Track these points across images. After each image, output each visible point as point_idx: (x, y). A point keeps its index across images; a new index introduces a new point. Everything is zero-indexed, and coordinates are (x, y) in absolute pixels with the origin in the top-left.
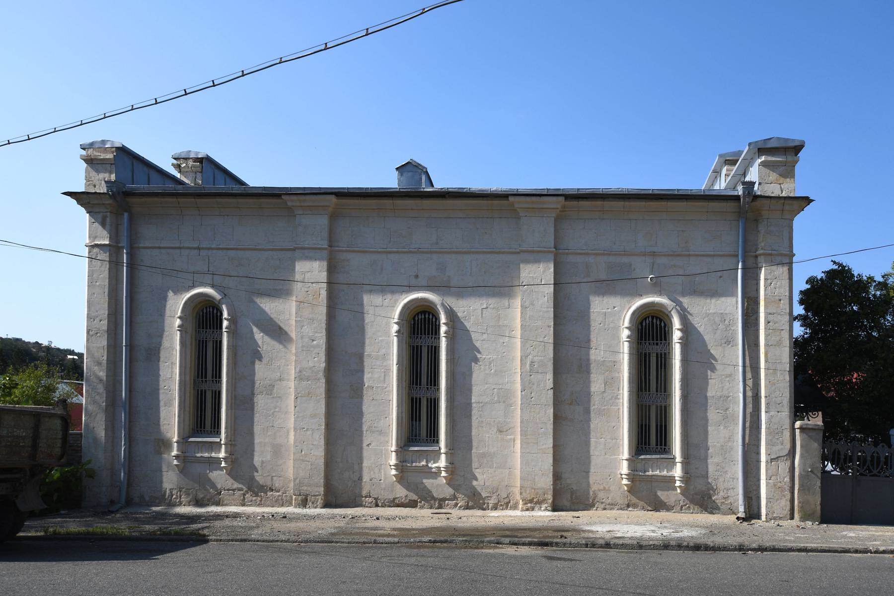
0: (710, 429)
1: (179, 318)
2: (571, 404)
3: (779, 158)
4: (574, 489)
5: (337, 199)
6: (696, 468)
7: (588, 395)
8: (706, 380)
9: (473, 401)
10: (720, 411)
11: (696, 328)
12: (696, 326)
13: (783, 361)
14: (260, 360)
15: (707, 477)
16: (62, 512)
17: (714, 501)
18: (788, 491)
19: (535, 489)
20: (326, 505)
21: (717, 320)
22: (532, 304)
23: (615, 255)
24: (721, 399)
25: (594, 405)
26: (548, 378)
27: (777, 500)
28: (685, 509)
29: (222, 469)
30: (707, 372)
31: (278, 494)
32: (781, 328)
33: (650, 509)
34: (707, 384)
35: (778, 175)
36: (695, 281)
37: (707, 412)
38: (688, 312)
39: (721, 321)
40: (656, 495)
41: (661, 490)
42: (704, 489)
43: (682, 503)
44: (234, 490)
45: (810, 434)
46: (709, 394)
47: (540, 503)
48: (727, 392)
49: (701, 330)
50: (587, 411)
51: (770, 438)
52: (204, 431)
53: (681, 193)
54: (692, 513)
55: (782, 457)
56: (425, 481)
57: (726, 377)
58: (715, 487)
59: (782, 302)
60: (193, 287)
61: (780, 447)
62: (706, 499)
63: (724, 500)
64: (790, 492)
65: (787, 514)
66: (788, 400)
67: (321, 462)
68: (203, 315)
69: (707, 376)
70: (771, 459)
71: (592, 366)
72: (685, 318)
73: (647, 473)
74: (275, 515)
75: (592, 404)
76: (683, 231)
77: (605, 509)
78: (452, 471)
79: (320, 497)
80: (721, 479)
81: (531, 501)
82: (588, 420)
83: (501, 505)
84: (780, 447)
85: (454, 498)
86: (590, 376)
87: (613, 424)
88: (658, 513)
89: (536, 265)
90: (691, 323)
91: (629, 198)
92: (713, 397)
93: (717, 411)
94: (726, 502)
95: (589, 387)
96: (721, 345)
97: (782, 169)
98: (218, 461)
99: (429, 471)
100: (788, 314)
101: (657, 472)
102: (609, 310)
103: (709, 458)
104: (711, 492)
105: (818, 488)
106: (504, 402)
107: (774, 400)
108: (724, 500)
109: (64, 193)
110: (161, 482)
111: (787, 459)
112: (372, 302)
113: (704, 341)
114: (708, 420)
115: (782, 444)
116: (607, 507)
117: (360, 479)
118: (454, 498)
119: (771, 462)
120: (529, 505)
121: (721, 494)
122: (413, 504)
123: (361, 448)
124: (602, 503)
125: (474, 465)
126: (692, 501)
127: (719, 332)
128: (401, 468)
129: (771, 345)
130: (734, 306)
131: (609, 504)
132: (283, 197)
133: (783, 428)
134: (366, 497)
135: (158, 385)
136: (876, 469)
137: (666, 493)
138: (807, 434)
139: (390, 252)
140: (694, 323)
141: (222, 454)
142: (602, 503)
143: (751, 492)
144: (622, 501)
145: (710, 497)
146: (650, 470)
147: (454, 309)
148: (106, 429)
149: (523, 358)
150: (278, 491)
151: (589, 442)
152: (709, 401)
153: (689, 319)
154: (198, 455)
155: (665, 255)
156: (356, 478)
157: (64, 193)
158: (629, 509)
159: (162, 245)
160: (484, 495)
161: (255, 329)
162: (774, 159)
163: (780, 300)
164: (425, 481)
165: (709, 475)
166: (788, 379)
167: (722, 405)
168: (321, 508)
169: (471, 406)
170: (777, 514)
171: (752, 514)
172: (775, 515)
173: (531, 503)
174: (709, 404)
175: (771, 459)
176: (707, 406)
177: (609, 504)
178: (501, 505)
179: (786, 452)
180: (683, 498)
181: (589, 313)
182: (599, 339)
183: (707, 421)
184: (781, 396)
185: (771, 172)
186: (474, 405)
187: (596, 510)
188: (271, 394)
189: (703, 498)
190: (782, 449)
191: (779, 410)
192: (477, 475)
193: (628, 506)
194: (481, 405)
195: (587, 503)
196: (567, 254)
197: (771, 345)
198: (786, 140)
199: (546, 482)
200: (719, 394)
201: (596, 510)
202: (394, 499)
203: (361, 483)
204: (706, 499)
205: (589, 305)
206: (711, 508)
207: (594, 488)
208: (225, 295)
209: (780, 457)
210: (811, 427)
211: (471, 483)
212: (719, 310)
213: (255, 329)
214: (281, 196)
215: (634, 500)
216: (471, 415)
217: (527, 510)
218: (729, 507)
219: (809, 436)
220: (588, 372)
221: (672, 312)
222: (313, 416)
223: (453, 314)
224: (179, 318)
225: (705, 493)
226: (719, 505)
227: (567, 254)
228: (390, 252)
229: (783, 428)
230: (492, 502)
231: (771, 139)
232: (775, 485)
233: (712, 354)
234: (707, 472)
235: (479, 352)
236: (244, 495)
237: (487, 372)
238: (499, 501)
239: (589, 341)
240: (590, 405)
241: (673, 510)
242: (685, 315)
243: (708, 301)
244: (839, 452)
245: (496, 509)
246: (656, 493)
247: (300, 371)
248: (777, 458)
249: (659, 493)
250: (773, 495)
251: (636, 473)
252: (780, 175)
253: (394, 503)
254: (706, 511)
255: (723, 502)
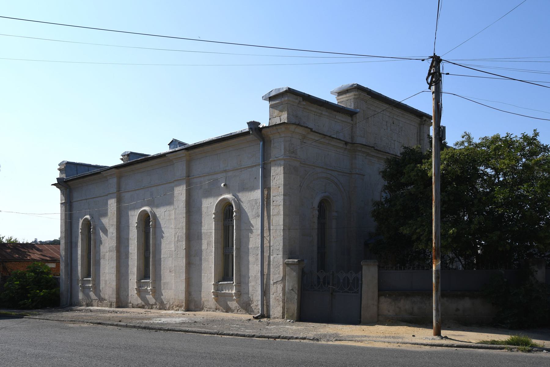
0: (250, 266)
1: (214, 214)
2: (195, 256)
3: (277, 101)
4: (196, 300)
5: (187, 151)
6: (244, 289)
7: (201, 251)
8: (248, 238)
9: (162, 257)
10: (254, 256)
11: (244, 209)
12: (244, 208)
13: (280, 224)
14: (102, 244)
15: (249, 295)
16: (48, 307)
17: (251, 307)
18: (282, 301)
19: (179, 300)
20: (118, 307)
21: (254, 203)
22: (178, 207)
23: (211, 175)
24: (255, 249)
25: (203, 256)
26: (183, 244)
27: (276, 307)
28: (239, 312)
29: (234, 300)
30: (249, 234)
31: (106, 301)
32: (279, 204)
33: (224, 311)
34: (249, 241)
35: (279, 111)
36: (244, 182)
37: (249, 257)
38: (241, 201)
39: (255, 203)
40: (227, 304)
41: (229, 301)
42: (247, 301)
43: (238, 309)
44: (95, 300)
45: (291, 267)
46: (250, 247)
47: (181, 307)
48: (257, 245)
49: (246, 210)
50: (201, 259)
51: (273, 270)
52: (228, 278)
53: (232, 134)
54: (242, 314)
55: (279, 281)
56: (147, 296)
57: (257, 236)
58: (252, 299)
59: (280, 188)
60: (141, 208)
61: (278, 275)
62: (248, 306)
63: (256, 307)
64: (283, 303)
65: (281, 316)
66: (282, 247)
67: (115, 287)
68: (226, 211)
69: (249, 236)
70: (274, 283)
71: (203, 235)
72: (239, 205)
73: (222, 292)
74: (169, 317)
75: (202, 256)
76: (239, 155)
77: (207, 311)
78: (154, 291)
79: (115, 303)
80: (255, 295)
81: (178, 306)
82: (201, 264)
83: (171, 308)
84: (278, 275)
85: (156, 304)
86: (202, 241)
87: (210, 266)
88: (227, 313)
89: (180, 187)
90: (242, 207)
91: (196, 148)
92: (251, 248)
93: (253, 256)
94: (257, 308)
95: (201, 247)
96: (255, 218)
97: (280, 107)
98: (231, 295)
99: (147, 291)
100: (283, 195)
101: (227, 291)
102: (209, 205)
103: (249, 283)
104: (251, 302)
105: (296, 300)
106: (172, 257)
107: (275, 248)
108: (256, 307)
109: (52, 185)
110: (79, 297)
111: (281, 283)
112: (131, 213)
113: (248, 216)
114: (249, 261)
115: (279, 274)
116: (208, 310)
117: (128, 295)
118: (156, 304)
119: (274, 285)
120: (177, 308)
121: (255, 303)
122: (143, 307)
123: (128, 281)
124: (206, 307)
125: (162, 288)
126: (242, 307)
127: (254, 210)
128: (138, 290)
129: (275, 215)
130: (257, 194)
131: (209, 308)
132: (102, 173)
133: (279, 264)
134: (130, 303)
135: (77, 257)
136: (357, 289)
137: (231, 302)
138: (290, 267)
139: (136, 190)
140: (243, 206)
141: (234, 292)
142: (206, 307)
143: (268, 302)
144: (214, 307)
145: (250, 305)
146: (224, 290)
147: (156, 213)
148: (65, 276)
149: (175, 234)
150: (106, 301)
151: (201, 275)
152: (250, 250)
153: (241, 205)
154: (86, 285)
155: (231, 171)
156: (127, 295)
157: (52, 185)
158: (217, 311)
159: (77, 200)
160: (165, 303)
161: (100, 231)
162: (277, 102)
163: (279, 187)
164: (147, 296)
165: (249, 292)
166: (282, 234)
167: (255, 253)
168: (115, 308)
169: (161, 260)
170: (276, 315)
171: (265, 315)
172: (275, 316)
173: (178, 307)
174: (250, 252)
175: (274, 283)
176: (249, 254)
177: (209, 308)
178: (171, 308)
179: (281, 279)
180: (238, 306)
181: (201, 207)
182: (205, 221)
183: (249, 261)
184: (279, 245)
185: (275, 110)
186: (162, 259)
187: (204, 311)
188: (104, 259)
189: (247, 306)
190: (279, 277)
191: (277, 254)
192: (163, 293)
193: (216, 310)
194: (164, 259)
195: (200, 307)
196: (193, 178)
197: (275, 215)
198: (279, 89)
199: (182, 296)
200: (254, 246)
201: (204, 311)
202: (138, 304)
203: (128, 297)
204: (248, 306)
205: (202, 203)
206: (250, 311)
207: (203, 299)
208: (93, 218)
209: (278, 281)
210: (290, 263)
211: (161, 297)
212: (255, 198)
213: (100, 231)
214: (165, 155)
215: (219, 306)
216: (161, 264)
217: (176, 310)
218: (258, 311)
219: (291, 268)
220: (201, 239)
221: (232, 202)
222: (113, 268)
223: (240, 206)
224: (214, 214)
225: (248, 302)
226: (254, 309)
227: (193, 178)
228: (136, 190)
229: (279, 264)
230: (168, 306)
231: (272, 91)
232: (275, 298)
233: (251, 224)
234: (249, 290)
235: (164, 233)
236: (98, 302)
237: (166, 242)
238: (170, 306)
239: (201, 223)
240: (202, 256)
241: (234, 312)
242: (239, 203)
243: (250, 193)
244: (348, 278)
245: (169, 310)
246: (227, 302)
247: (109, 248)
248: (277, 282)
249: (228, 303)
250: (274, 304)
251: (217, 292)
252: (280, 111)
253: (139, 307)
254: (248, 313)
255: (256, 308)
